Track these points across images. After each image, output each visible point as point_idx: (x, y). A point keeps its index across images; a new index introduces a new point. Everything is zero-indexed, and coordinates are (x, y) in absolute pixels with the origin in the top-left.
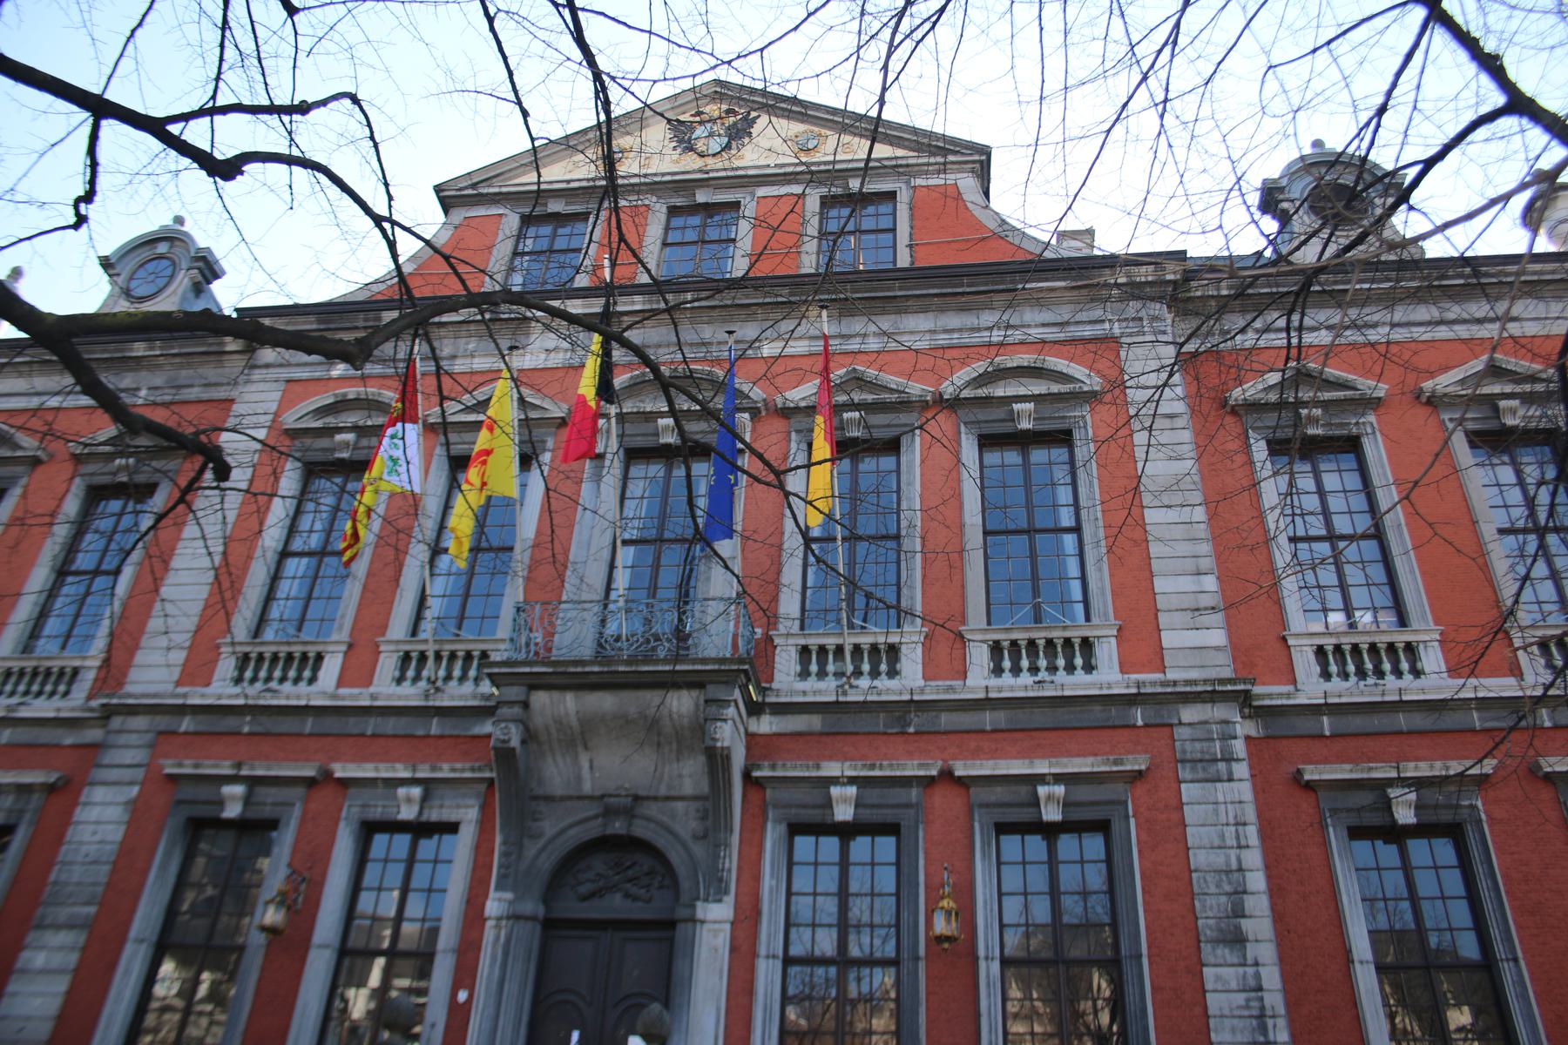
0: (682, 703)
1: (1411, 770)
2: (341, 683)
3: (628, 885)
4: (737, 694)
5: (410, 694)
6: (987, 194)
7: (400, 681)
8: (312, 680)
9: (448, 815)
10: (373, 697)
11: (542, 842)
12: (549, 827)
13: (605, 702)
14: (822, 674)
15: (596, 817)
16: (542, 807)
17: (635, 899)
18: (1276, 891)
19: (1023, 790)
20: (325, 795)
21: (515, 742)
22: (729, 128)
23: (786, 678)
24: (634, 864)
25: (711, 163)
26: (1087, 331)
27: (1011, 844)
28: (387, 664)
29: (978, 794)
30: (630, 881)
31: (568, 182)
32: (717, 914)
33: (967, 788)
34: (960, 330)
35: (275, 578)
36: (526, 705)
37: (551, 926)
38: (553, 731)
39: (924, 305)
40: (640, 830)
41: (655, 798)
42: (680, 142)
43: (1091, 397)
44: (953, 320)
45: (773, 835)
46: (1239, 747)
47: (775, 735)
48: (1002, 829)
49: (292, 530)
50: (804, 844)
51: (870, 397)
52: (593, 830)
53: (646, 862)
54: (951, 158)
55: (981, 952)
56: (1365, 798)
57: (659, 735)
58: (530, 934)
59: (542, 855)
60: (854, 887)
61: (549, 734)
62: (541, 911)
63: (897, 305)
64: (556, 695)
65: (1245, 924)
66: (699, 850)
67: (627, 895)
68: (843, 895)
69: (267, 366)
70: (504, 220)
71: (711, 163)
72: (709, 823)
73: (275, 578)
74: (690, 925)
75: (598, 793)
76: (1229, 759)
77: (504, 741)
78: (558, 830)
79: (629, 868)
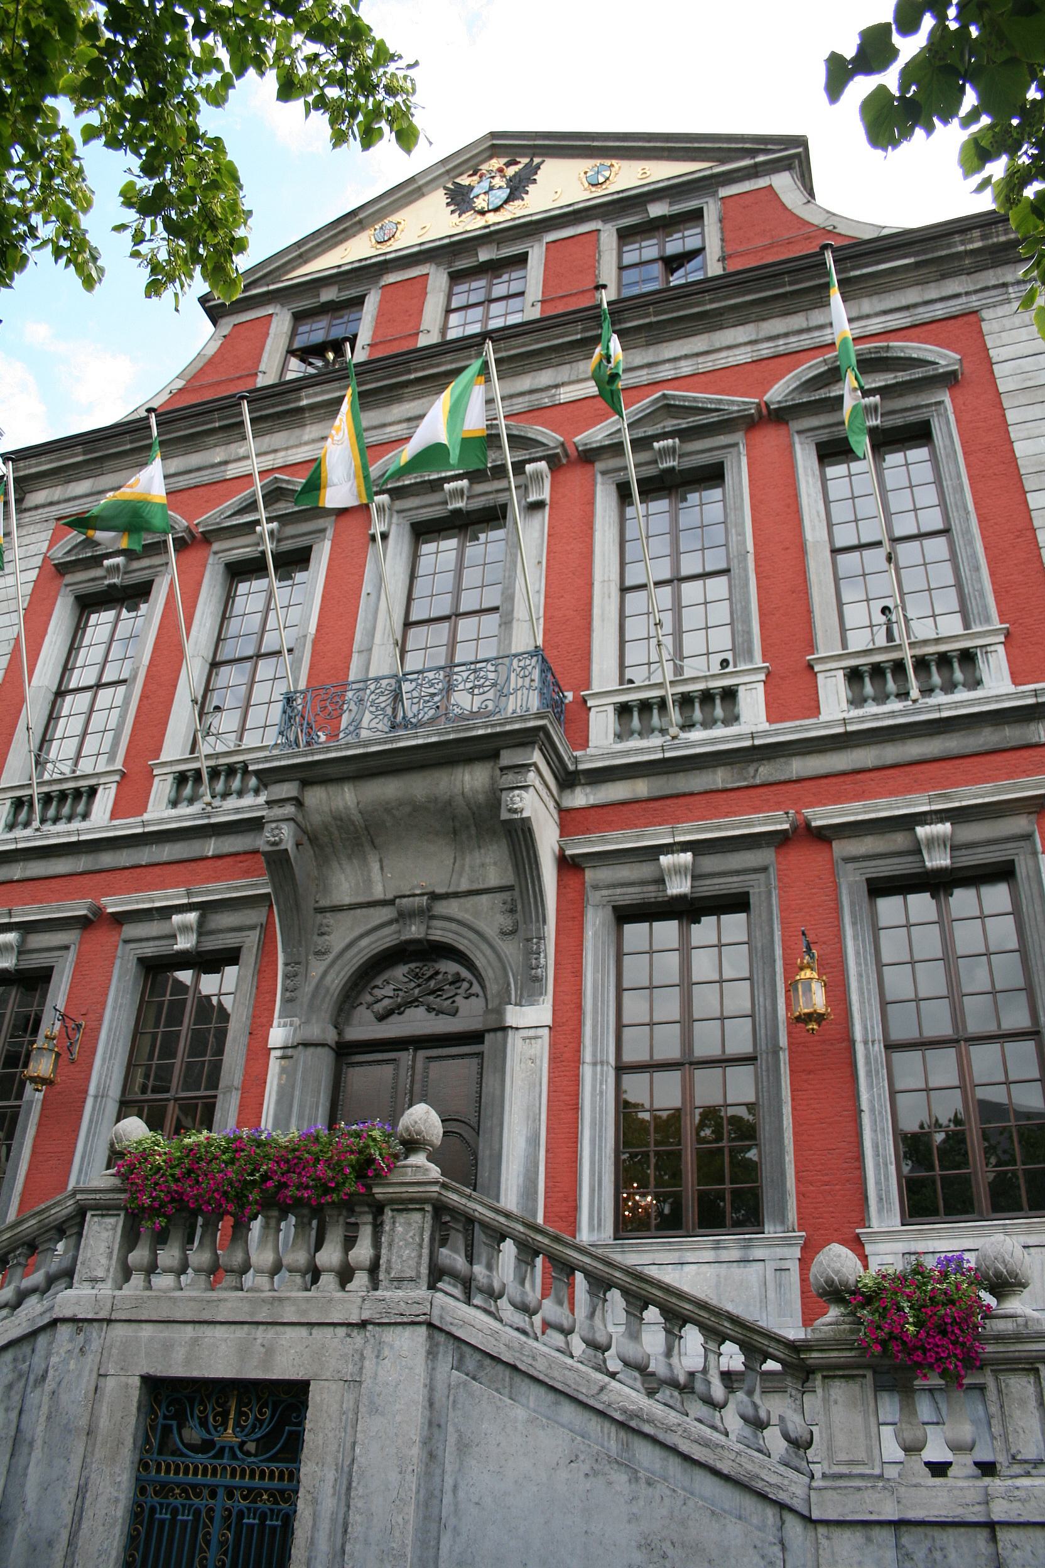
0: (472, 780)
2: (114, 815)
3: (431, 998)
4: (537, 757)
5: (187, 814)
6: (811, 194)
7: (174, 803)
8: (85, 816)
9: (228, 941)
10: (144, 824)
11: (330, 958)
12: (337, 939)
13: (387, 789)
15: (390, 923)
16: (330, 919)
17: (439, 1012)
20: (101, 937)
21: (289, 845)
22: (510, 180)
23: (603, 739)
24: (437, 973)
25: (492, 218)
26: (939, 310)
27: (889, 907)
28: (162, 788)
29: (842, 848)
30: (432, 992)
31: (339, 266)
32: (532, 1016)
33: (829, 842)
34: (786, 335)
35: (52, 717)
36: (298, 802)
37: (345, 1052)
38: (334, 830)
39: (740, 315)
40: (440, 933)
41: (456, 895)
43: (949, 380)
44: (777, 325)
45: (596, 922)
47: (593, 807)
48: (879, 888)
49: (67, 669)
50: (635, 933)
51: (684, 424)
52: (387, 939)
53: (450, 967)
54: (761, 158)
55: (858, 1035)
57: (454, 818)
59: (329, 974)
60: (674, 958)
61: (330, 834)
62: (331, 1036)
63: (710, 322)
64: (332, 789)
66: (510, 949)
67: (430, 1009)
68: (949, 957)
69: (36, 508)
70: (275, 319)
71: (492, 218)
72: (519, 916)
73: (52, 717)
74: (499, 1034)
75: (389, 896)
77: (275, 844)
79: (431, 978)
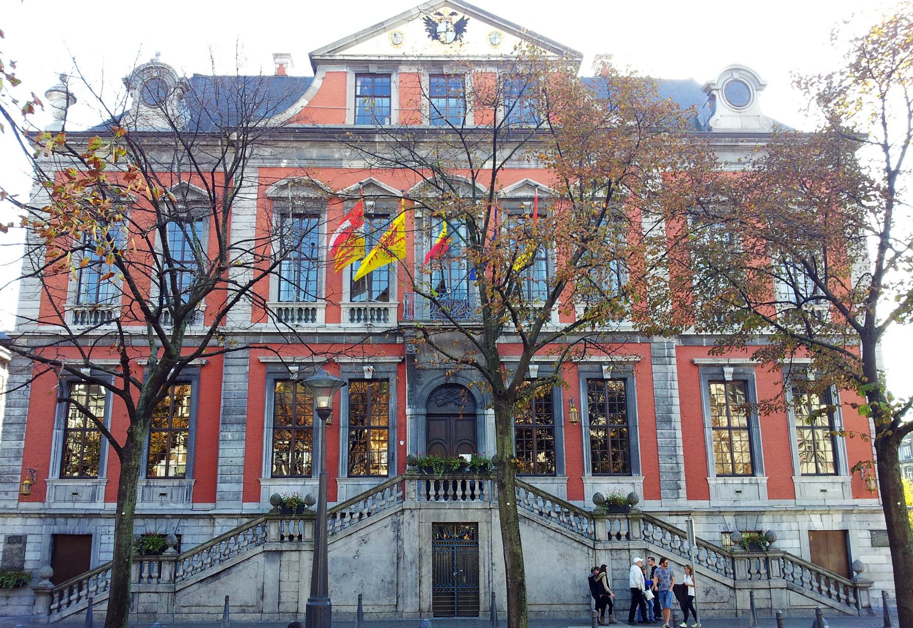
1: (732, 361)
5: (358, 327)
14: (359, 320)
18: (682, 403)
19: (597, 366)
40: (460, 381)
42: (431, 31)
46: (674, 352)
52: (442, 381)
56: (716, 370)
58: (422, 419)
59: (423, 390)
65: (673, 416)
76: (670, 357)
78: (430, 381)
